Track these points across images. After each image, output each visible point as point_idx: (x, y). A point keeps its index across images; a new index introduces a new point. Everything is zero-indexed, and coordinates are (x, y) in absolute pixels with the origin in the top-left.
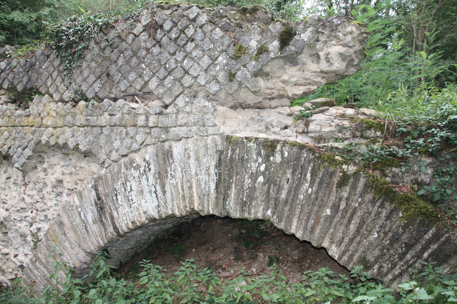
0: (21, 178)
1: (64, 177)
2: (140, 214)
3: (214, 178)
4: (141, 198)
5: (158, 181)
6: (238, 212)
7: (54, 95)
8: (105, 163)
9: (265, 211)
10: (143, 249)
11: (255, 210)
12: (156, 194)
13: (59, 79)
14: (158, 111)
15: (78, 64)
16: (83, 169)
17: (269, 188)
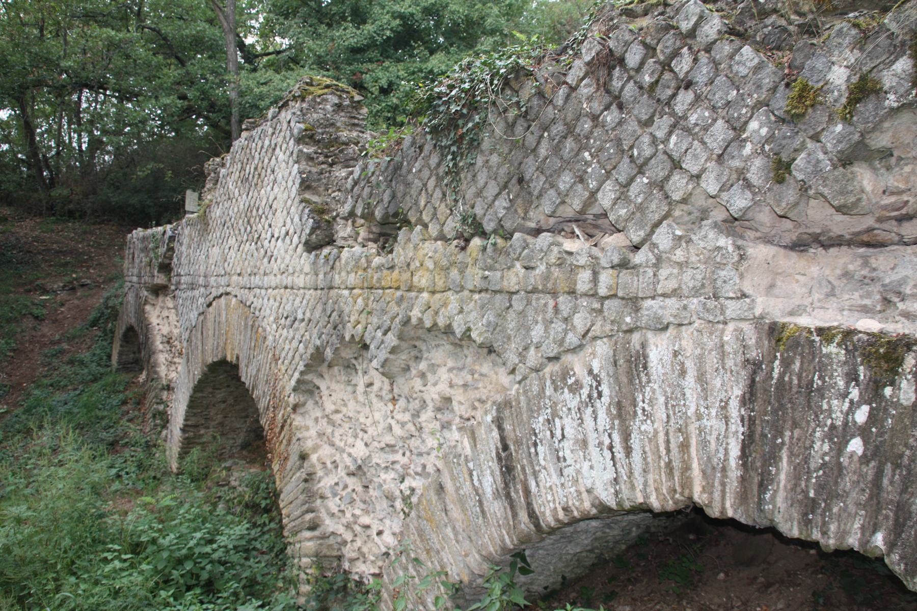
0: (387, 387)
1: (452, 392)
2: (579, 493)
3: (738, 429)
4: (582, 457)
5: (617, 422)
6: (795, 523)
7: (430, 225)
8: (517, 372)
9: (867, 534)
10: (616, 552)
11: (839, 528)
12: (613, 453)
13: (438, 194)
14: (616, 261)
15: (469, 161)
17: (879, 474)
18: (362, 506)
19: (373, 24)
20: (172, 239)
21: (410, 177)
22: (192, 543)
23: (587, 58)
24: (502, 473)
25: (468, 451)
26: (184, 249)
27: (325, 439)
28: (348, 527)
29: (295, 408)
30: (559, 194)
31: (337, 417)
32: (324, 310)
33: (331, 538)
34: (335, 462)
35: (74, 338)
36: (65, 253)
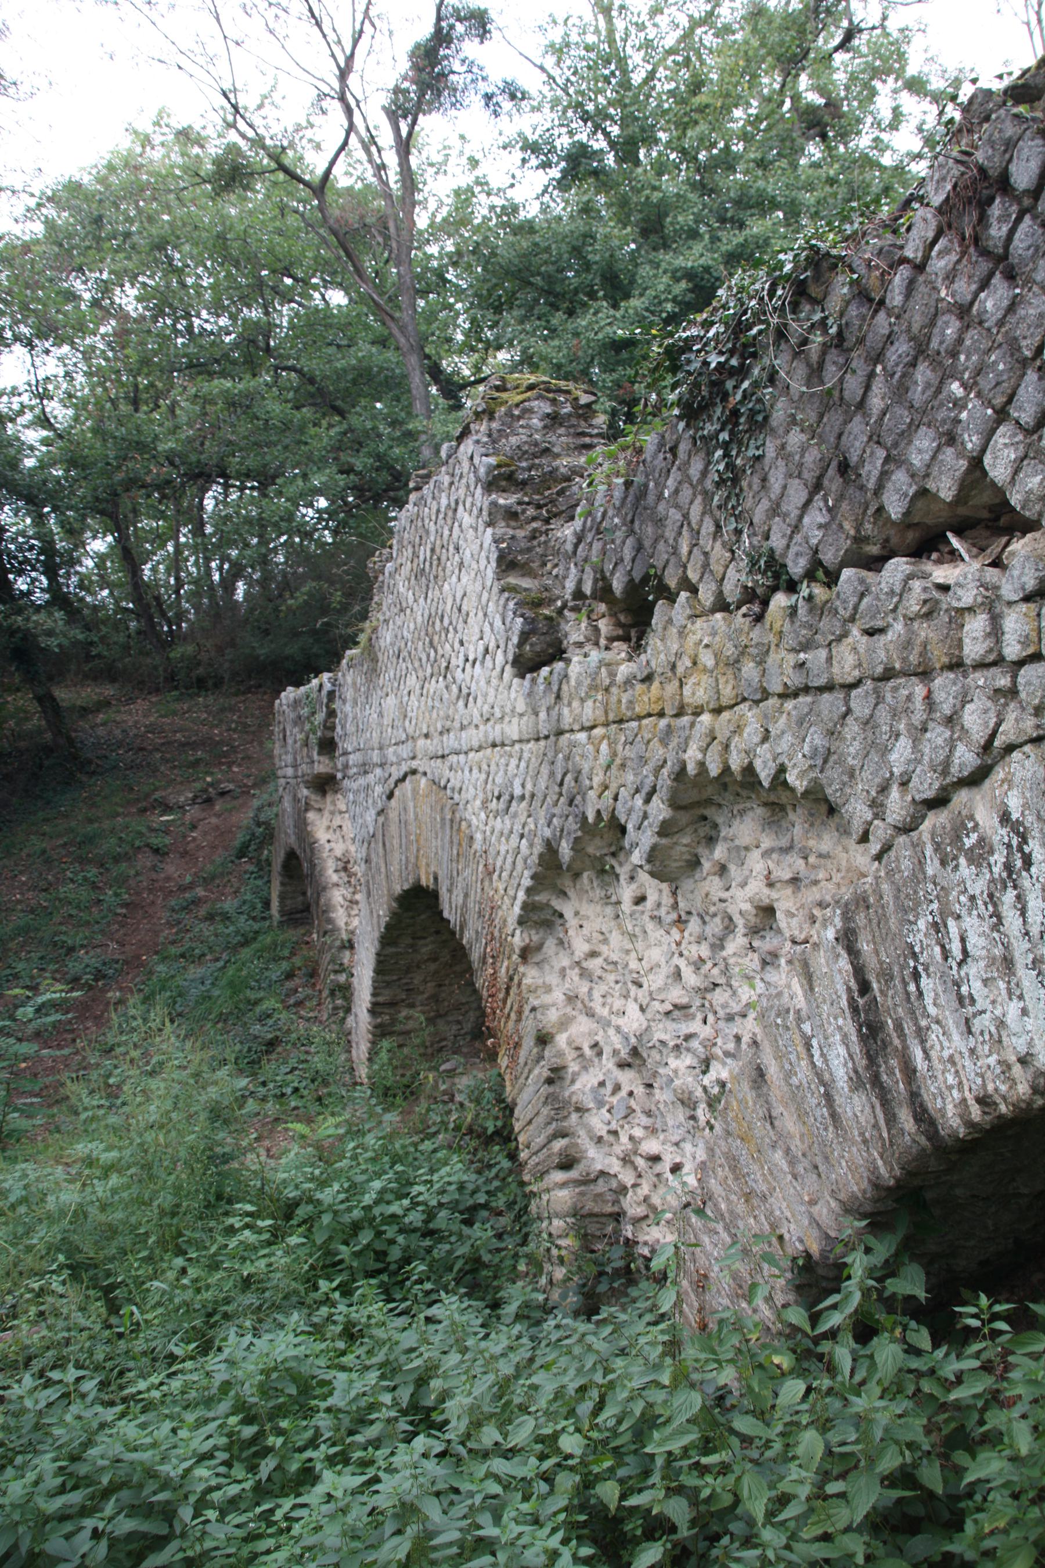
0: (667, 900)
1: (774, 895)
2: (1006, 1066)
4: (1004, 992)
13: (708, 527)
15: (751, 453)
16: (828, 862)
18: (645, 1120)
19: (641, 295)
20: (331, 695)
21: (661, 507)
22: (368, 1199)
23: (937, 200)
24: (863, 1038)
25: (800, 1001)
26: (348, 708)
27: (579, 1005)
28: (626, 1161)
29: (525, 954)
30: (913, 476)
31: (594, 965)
32: (552, 774)
33: (601, 1181)
34: (596, 1045)
35: (213, 878)
36: (193, 746)
